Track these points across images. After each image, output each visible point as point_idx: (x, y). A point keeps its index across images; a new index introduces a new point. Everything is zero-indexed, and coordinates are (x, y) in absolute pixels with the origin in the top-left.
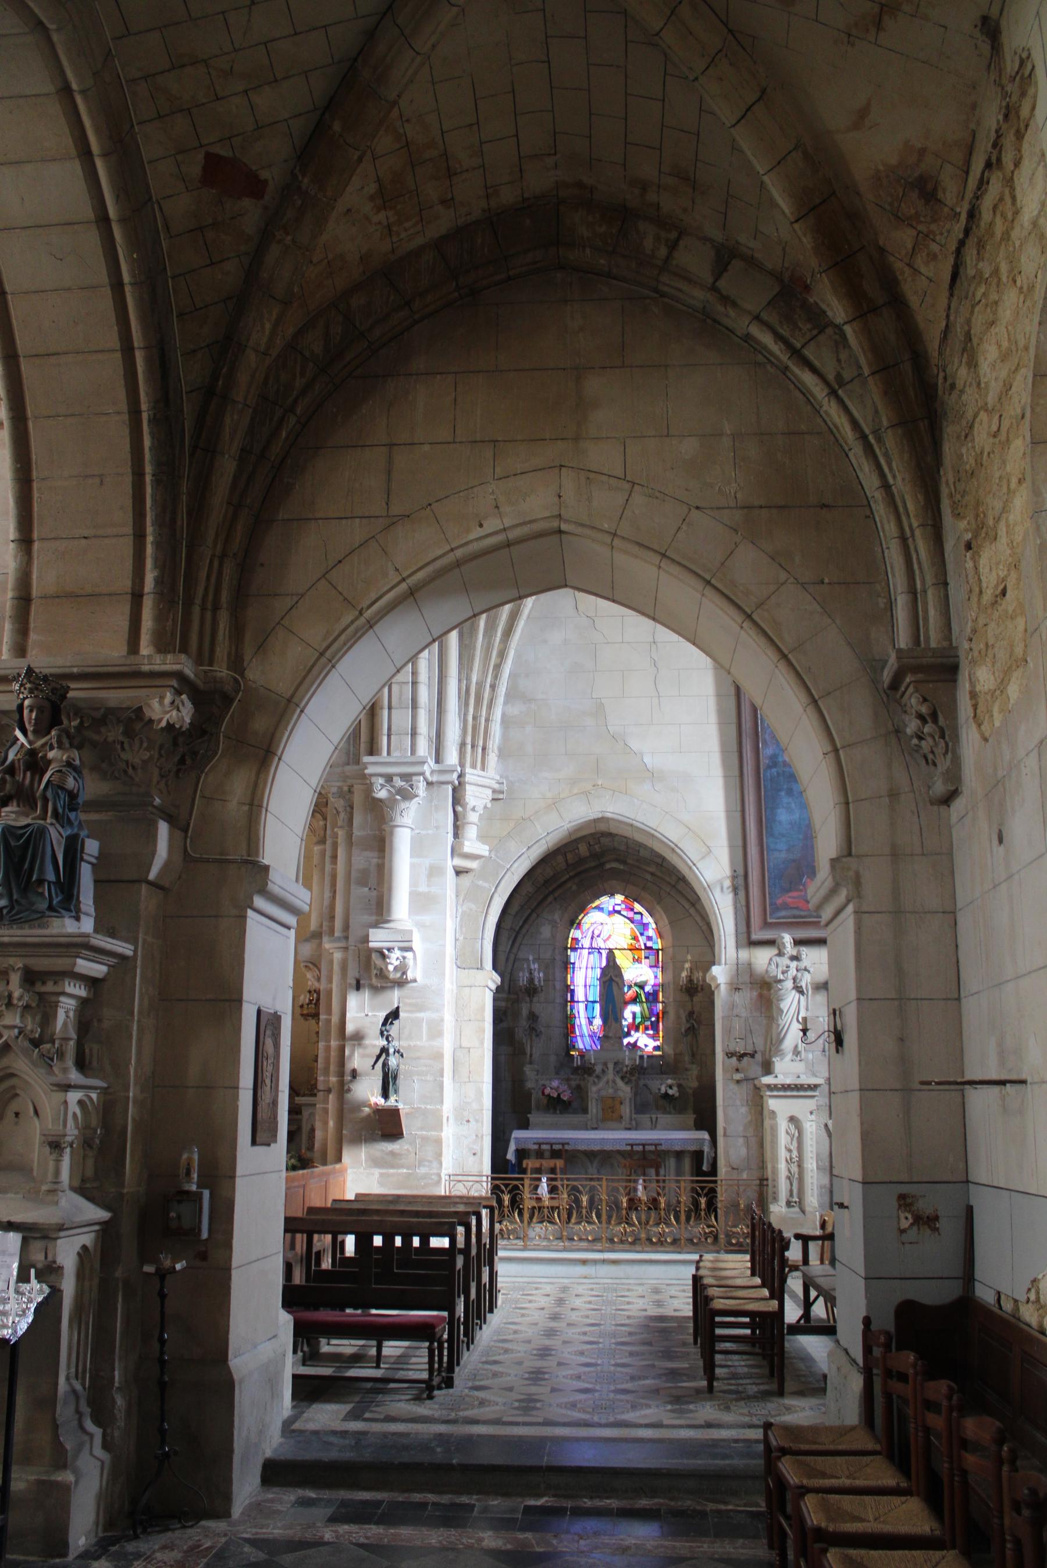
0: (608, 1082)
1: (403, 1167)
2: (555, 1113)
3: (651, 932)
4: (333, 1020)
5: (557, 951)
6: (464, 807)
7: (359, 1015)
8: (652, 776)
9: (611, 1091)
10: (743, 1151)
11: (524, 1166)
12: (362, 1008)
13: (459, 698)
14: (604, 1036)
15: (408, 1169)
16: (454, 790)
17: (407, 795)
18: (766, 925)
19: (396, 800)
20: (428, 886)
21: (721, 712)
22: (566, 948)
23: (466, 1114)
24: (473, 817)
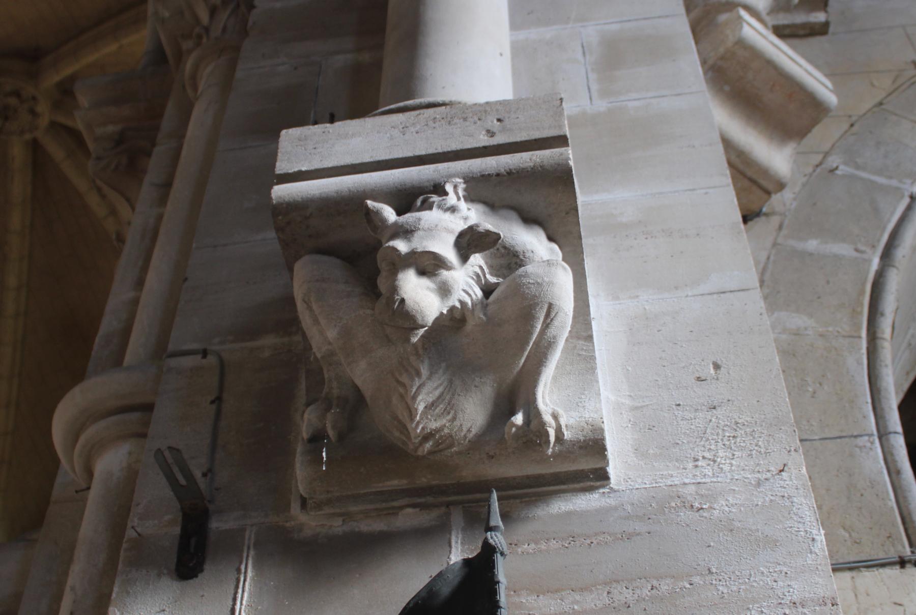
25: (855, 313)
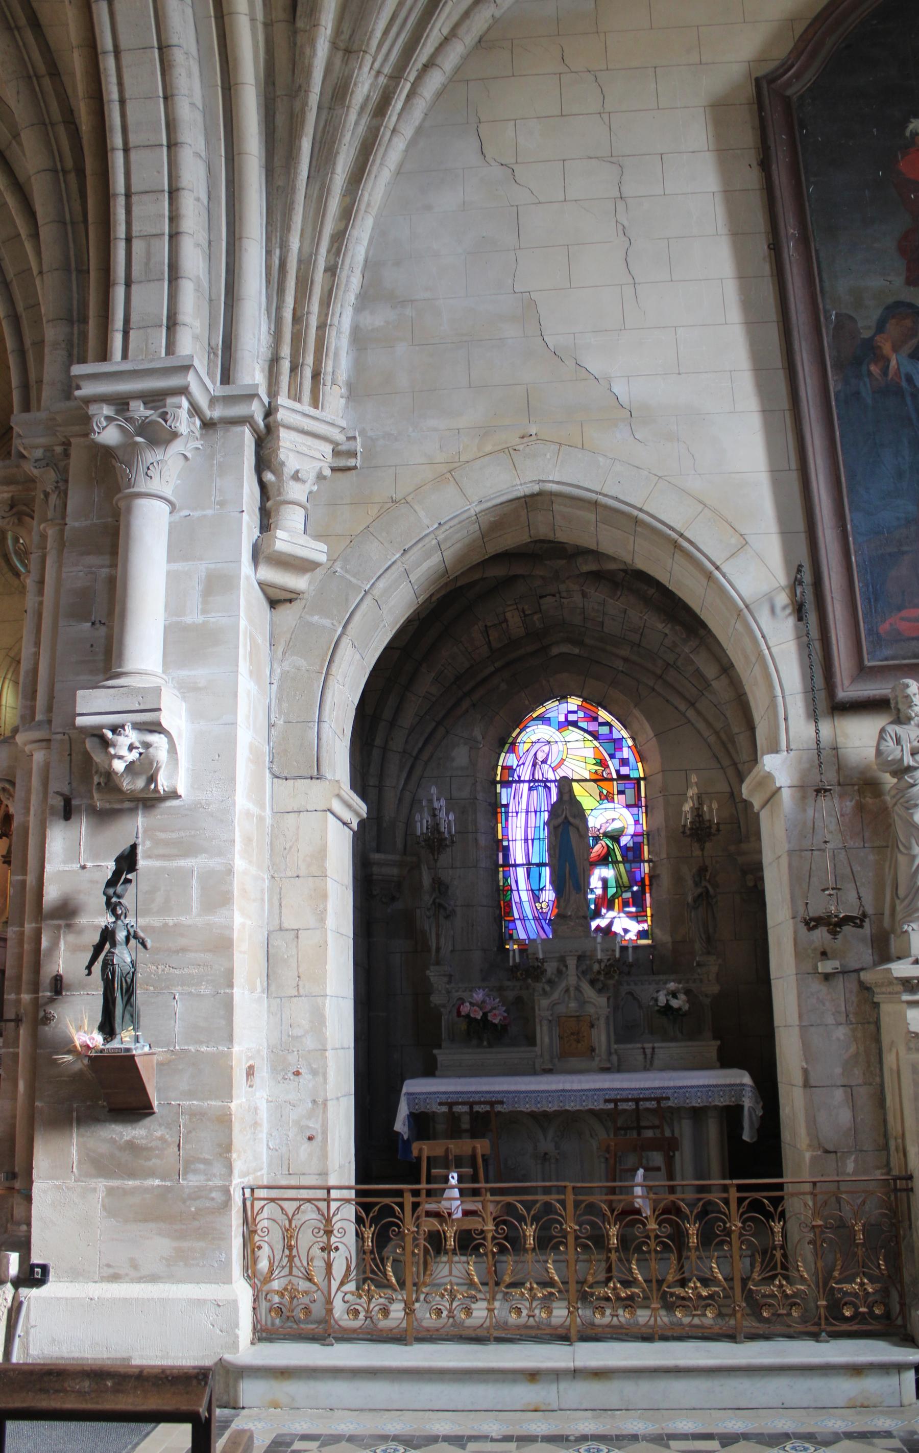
0: (567, 991)
1: (152, 1174)
2: (480, 1045)
3: (626, 753)
4: (28, 883)
5: (479, 788)
6: (278, 473)
7: (67, 868)
8: (629, 415)
9: (573, 1005)
10: (845, 1116)
11: (415, 1153)
12: (73, 854)
13: (268, 281)
14: (558, 916)
15: (163, 1179)
16: (260, 443)
17: (159, 436)
18: (862, 671)
19: (137, 444)
20: (204, 611)
21: (748, 304)
22: (495, 783)
23: (292, 1058)
24: (296, 492)
25: (324, 660)
